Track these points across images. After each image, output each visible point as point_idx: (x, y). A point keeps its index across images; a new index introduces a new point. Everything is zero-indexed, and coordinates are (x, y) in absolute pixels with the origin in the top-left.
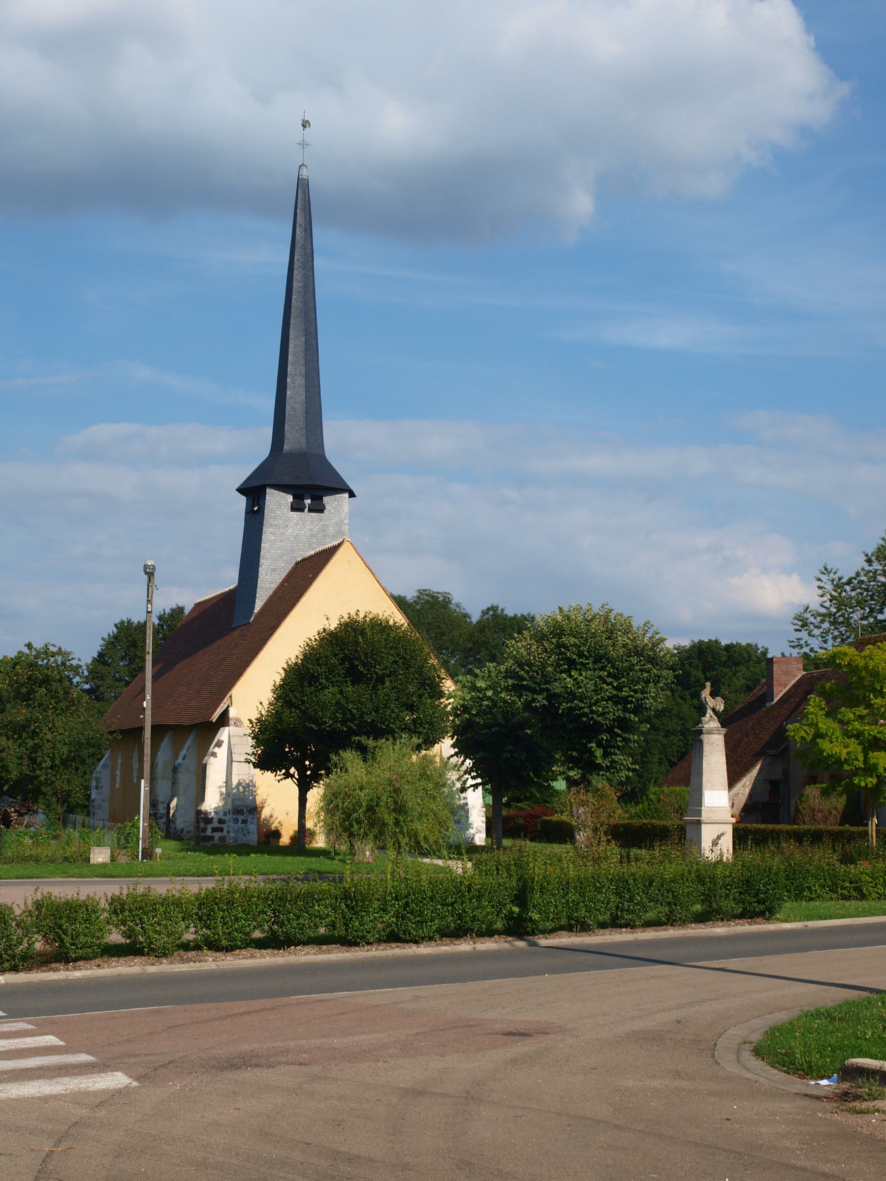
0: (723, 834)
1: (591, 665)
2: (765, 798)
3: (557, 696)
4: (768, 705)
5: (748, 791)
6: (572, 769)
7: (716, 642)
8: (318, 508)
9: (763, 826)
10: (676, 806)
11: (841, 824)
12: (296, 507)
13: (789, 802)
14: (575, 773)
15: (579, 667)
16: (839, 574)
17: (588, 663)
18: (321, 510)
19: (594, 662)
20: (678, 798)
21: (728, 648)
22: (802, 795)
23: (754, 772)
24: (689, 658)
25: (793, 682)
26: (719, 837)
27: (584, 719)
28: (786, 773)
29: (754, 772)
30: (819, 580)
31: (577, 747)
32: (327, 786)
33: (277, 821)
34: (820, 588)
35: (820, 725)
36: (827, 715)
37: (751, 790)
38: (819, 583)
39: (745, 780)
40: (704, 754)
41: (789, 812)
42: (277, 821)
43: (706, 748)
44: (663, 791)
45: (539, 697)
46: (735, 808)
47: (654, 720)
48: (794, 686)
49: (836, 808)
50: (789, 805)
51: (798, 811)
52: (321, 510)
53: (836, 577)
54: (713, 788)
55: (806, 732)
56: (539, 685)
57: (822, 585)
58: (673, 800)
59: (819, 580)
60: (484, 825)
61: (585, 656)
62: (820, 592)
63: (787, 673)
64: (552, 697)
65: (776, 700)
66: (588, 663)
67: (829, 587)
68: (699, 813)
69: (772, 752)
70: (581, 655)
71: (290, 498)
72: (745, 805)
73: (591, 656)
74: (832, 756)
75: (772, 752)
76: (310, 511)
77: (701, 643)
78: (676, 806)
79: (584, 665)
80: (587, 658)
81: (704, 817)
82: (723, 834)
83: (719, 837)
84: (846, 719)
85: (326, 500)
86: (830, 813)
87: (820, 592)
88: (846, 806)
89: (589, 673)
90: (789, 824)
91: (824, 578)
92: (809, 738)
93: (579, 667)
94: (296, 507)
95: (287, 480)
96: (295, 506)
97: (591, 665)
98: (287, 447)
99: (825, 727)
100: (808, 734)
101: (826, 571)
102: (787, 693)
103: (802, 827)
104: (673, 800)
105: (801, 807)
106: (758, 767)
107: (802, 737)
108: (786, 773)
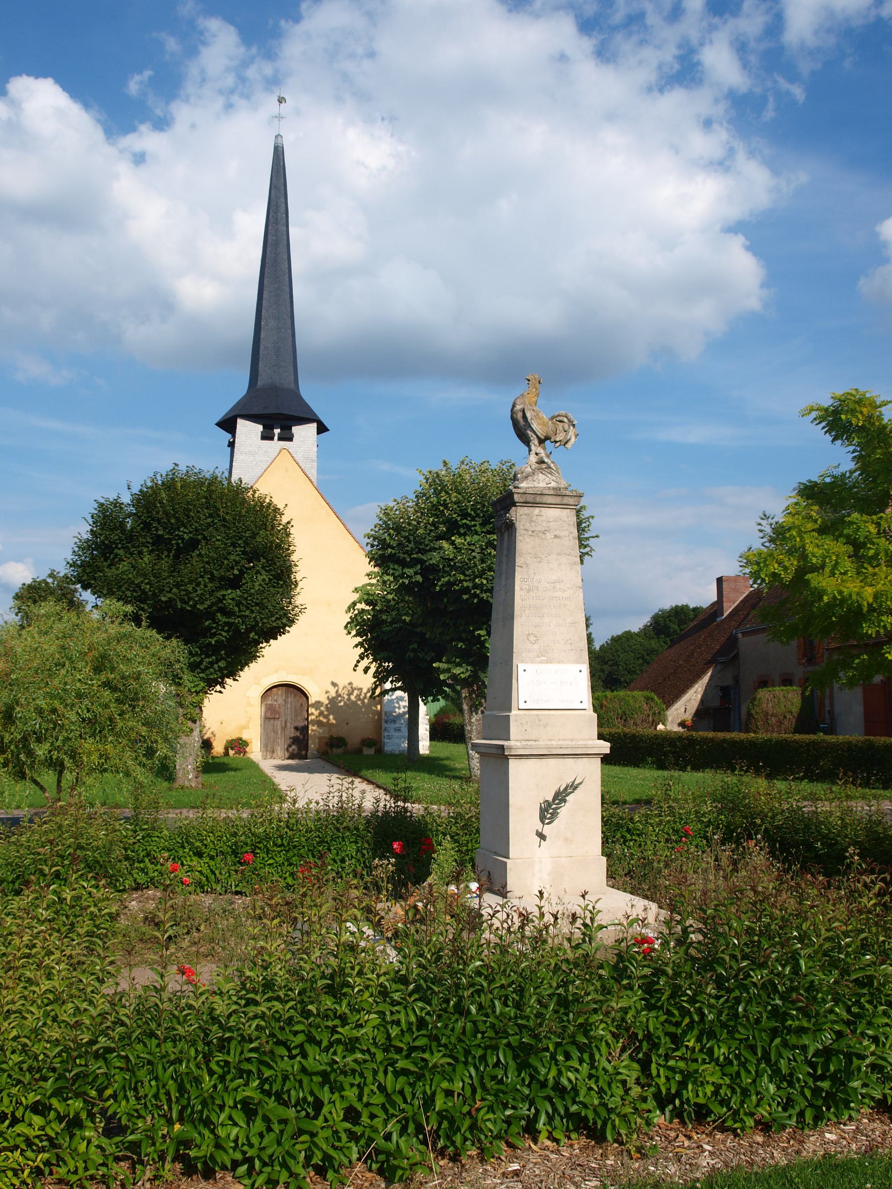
0: (573, 787)
1: (478, 528)
2: (716, 703)
3: (434, 569)
4: (719, 619)
5: (699, 696)
6: (459, 665)
7: (687, 606)
8: (287, 437)
9: (711, 734)
10: (620, 711)
11: (796, 731)
12: (267, 436)
13: (739, 706)
14: (462, 670)
15: (462, 531)
16: (776, 519)
17: (475, 525)
18: (290, 439)
19: (483, 525)
20: (622, 704)
21: (695, 609)
22: (754, 699)
23: (706, 679)
24: (669, 617)
25: (741, 599)
26: (561, 797)
27: (465, 597)
28: (736, 679)
29: (706, 679)
30: (759, 524)
31: (464, 636)
32: (447, 705)
33: (210, 732)
34: (761, 531)
35: (810, 548)
36: (822, 531)
37: (703, 696)
38: (760, 527)
39: (697, 686)
40: (519, 561)
41: (740, 716)
42: (210, 732)
43: (524, 544)
44: (606, 696)
45: (409, 571)
46: (687, 713)
47: (646, 657)
48: (742, 601)
49: (791, 712)
50: (740, 710)
51: (750, 715)
52: (290, 439)
53: (773, 521)
54: (545, 656)
55: (780, 563)
56: (409, 553)
57: (762, 528)
58: (617, 706)
59: (759, 524)
60: (428, 733)
61: (470, 515)
62: (761, 535)
63: (735, 590)
64: (429, 571)
65: (725, 615)
66: (475, 525)
67: (768, 530)
68: (502, 728)
69: (722, 659)
70: (465, 515)
71: (260, 428)
72: (697, 711)
73: (478, 515)
74: (843, 601)
75: (722, 659)
76: (280, 439)
77: (677, 607)
78: (620, 711)
79: (468, 527)
80: (473, 519)
81: (516, 741)
82: (573, 787)
83: (561, 797)
84: (861, 536)
85: (296, 430)
86: (785, 717)
87: (761, 535)
88: (800, 709)
89: (476, 537)
90: (740, 731)
91: (764, 522)
92: (787, 577)
93: (462, 531)
94: (267, 436)
95: (256, 411)
96: (265, 435)
97: (478, 528)
98: (260, 383)
99: (819, 552)
100: (786, 569)
101: (765, 517)
102: (736, 608)
103: (759, 736)
104: (617, 706)
105: (753, 712)
106: (709, 674)
107: (774, 575)
108: (736, 679)
